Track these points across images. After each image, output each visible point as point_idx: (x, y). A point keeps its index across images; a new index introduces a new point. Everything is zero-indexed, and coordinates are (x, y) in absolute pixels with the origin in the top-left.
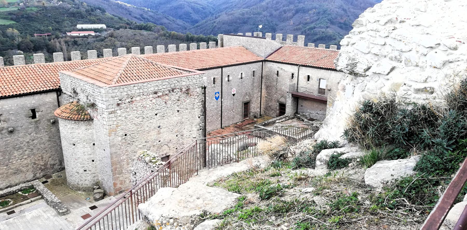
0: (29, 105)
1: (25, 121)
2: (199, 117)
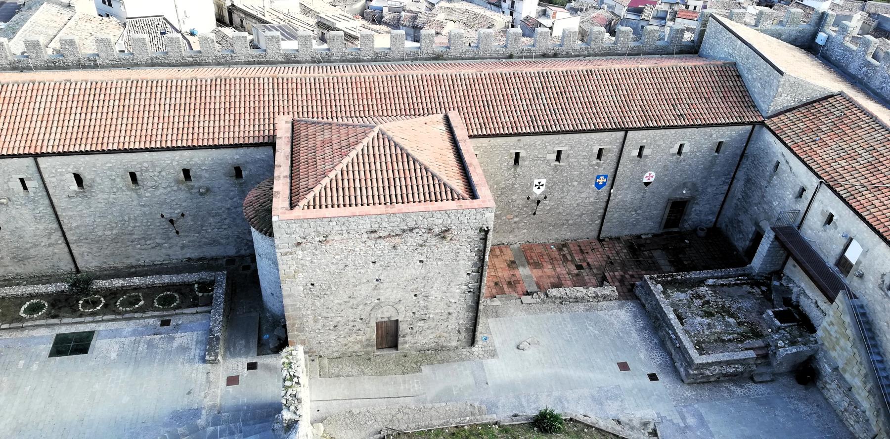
0: (230, 161)
2: (468, 274)
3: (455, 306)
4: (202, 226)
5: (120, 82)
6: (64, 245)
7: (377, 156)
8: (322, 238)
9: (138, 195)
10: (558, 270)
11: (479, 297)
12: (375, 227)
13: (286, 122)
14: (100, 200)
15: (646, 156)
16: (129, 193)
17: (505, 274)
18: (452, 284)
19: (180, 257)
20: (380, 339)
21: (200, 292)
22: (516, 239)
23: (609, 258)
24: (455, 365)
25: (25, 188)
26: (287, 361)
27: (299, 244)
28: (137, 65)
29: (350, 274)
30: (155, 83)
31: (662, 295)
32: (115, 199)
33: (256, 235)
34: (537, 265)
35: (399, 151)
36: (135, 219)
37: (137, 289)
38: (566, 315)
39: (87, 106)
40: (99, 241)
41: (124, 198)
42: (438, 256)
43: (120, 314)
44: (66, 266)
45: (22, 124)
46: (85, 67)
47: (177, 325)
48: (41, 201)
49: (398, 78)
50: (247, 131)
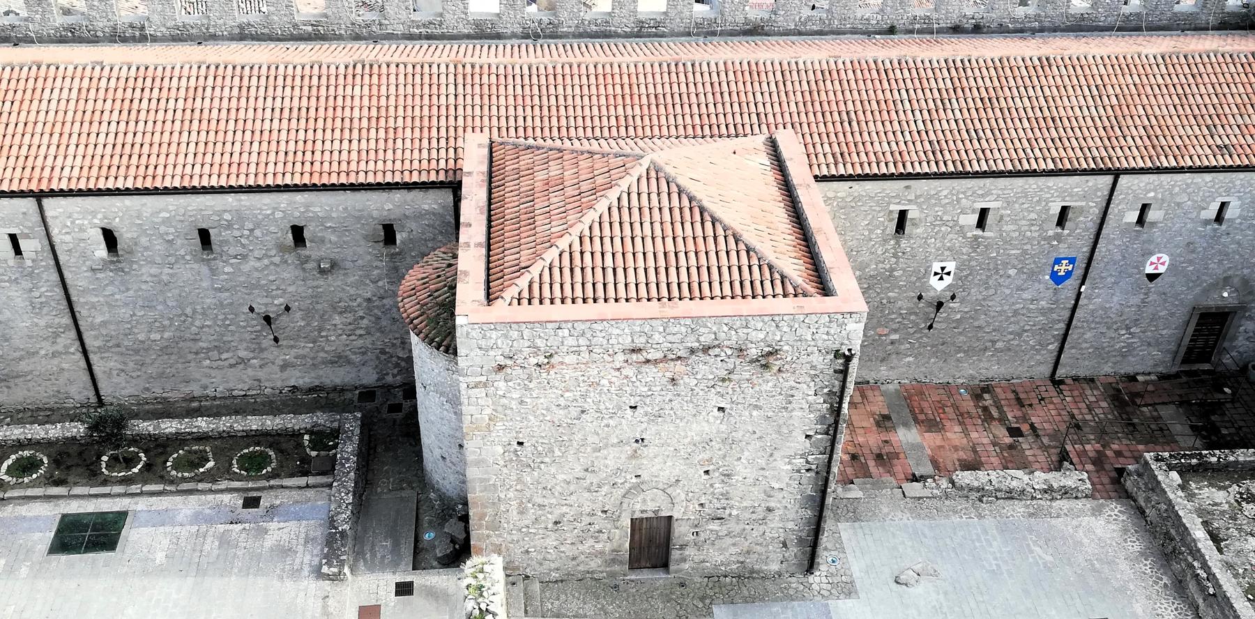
1: (365, 253)
2: (807, 436)
3: (780, 495)
4: (320, 330)
5: (187, 67)
6: (79, 356)
7: (646, 211)
8: (542, 360)
9: (211, 269)
10: (974, 435)
11: (827, 480)
12: (640, 341)
13: (480, 145)
14: (144, 278)
15: (1153, 224)
16: (196, 266)
17: (872, 440)
18: (777, 455)
19: (279, 384)
20: (636, 551)
21: (313, 449)
22: (893, 375)
23: (1073, 416)
24: (776, 608)
25: (18, 251)
26: (474, 582)
27: (501, 368)
28: (214, 37)
29: (590, 427)
30: (247, 69)
31: (1180, 493)
32: (171, 275)
33: (420, 349)
34: (932, 425)
35: (686, 202)
36: (203, 314)
37: (202, 438)
38: (989, 522)
39: (129, 109)
40: (140, 349)
41: (187, 275)
42: (753, 401)
43: (172, 483)
44: (80, 391)
45: (18, 137)
46: (124, 40)
47: (272, 507)
48: (45, 276)
49: (681, 68)
50: (413, 161)
